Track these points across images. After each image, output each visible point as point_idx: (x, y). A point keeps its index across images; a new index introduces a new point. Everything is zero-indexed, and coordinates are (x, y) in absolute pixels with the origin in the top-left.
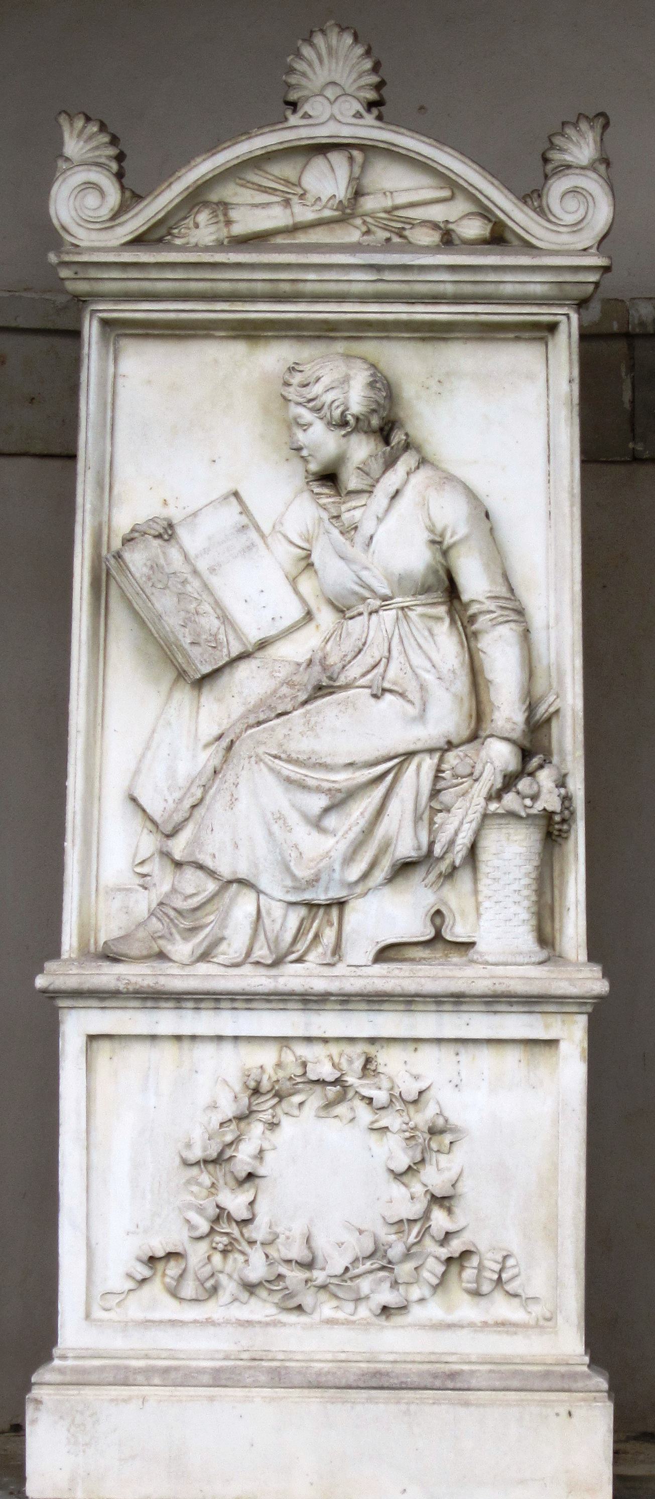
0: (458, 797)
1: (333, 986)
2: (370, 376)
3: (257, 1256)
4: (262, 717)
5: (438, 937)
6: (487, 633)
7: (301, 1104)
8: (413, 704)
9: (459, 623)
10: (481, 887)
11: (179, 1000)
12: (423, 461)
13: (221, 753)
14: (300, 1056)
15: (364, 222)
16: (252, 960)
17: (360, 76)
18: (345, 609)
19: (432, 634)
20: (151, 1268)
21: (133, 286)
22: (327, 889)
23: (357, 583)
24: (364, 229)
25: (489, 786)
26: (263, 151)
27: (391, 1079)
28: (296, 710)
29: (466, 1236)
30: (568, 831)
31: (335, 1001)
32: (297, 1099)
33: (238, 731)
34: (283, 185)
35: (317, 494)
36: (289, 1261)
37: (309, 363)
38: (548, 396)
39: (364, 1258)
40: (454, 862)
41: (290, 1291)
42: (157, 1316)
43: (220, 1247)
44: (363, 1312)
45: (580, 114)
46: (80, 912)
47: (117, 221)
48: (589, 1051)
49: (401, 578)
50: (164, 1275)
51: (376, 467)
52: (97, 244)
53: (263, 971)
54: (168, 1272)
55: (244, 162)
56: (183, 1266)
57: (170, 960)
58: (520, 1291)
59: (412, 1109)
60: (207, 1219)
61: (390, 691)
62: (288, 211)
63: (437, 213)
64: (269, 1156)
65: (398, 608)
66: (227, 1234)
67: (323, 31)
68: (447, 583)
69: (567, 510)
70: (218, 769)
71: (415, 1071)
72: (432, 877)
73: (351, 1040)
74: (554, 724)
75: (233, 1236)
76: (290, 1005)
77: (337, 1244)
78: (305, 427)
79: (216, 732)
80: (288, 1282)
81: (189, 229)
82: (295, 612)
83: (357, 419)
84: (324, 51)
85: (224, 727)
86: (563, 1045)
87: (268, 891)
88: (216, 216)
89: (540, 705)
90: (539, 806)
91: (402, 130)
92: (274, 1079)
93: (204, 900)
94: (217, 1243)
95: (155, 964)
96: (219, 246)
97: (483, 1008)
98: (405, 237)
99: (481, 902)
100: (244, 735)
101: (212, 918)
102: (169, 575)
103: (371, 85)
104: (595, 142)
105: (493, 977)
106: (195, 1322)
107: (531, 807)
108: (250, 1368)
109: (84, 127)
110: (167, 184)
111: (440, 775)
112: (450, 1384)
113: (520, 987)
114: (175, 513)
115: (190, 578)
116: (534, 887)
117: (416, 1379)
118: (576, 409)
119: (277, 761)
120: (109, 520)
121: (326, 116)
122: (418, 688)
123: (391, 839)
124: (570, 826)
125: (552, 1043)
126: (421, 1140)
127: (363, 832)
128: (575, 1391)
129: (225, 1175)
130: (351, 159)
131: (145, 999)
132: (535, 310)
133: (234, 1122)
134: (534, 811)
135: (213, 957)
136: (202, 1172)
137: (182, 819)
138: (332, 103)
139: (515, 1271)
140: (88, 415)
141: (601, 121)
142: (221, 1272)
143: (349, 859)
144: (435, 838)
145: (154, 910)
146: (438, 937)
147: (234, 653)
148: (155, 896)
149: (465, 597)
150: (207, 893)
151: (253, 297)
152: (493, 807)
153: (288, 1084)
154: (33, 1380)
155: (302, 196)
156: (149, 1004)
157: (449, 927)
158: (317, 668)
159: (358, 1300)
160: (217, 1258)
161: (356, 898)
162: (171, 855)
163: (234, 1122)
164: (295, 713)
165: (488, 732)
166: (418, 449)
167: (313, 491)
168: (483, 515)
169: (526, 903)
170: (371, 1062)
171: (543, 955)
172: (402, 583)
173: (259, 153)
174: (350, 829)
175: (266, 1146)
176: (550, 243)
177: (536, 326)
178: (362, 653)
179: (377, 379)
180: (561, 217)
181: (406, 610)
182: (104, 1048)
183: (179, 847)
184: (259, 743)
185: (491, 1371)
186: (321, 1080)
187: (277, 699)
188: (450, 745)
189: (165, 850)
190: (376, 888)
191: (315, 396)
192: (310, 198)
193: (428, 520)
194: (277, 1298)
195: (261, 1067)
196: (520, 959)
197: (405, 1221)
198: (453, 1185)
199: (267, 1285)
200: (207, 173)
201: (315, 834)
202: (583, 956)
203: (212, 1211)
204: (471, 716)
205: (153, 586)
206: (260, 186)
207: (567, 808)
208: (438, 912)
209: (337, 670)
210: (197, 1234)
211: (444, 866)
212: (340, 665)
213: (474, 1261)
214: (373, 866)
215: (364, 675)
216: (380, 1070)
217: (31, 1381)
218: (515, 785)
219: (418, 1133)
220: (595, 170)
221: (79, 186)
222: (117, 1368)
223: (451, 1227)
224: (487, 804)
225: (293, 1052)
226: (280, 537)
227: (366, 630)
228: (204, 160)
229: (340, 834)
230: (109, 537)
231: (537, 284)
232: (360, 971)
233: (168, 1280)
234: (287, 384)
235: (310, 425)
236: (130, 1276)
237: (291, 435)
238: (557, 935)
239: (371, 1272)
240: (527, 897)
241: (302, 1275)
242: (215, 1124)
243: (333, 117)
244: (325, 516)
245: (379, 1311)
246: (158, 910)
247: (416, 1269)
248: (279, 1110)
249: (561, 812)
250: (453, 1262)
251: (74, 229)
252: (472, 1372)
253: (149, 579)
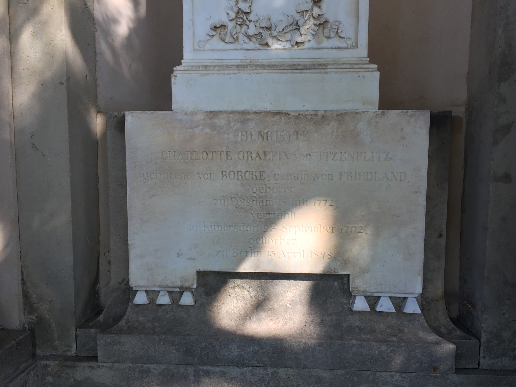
39: (289, 25)
66: (241, 18)
142: (240, 33)
160: (238, 27)
187: (268, 257)
203: (236, 10)
210: (231, 18)
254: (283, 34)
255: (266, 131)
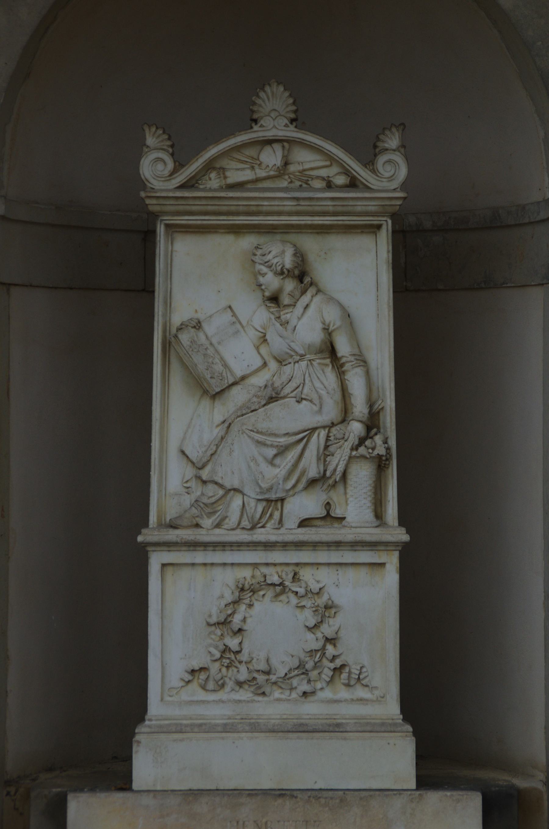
0: (337, 449)
1: (280, 539)
2: (294, 250)
3: (243, 669)
4: (244, 412)
5: (328, 515)
6: (350, 371)
7: (264, 595)
8: (316, 405)
9: (336, 367)
10: (348, 491)
11: (205, 546)
12: (319, 291)
13: (225, 429)
14: (263, 573)
15: (289, 177)
16: (241, 526)
17: (287, 106)
18: (282, 361)
19: (324, 372)
20: (192, 675)
21: (181, 208)
22: (276, 493)
23: (288, 349)
24: (289, 180)
25: (352, 443)
26: (241, 143)
27: (306, 583)
28: (260, 408)
29: (343, 657)
30: (389, 464)
31: (280, 546)
32: (262, 593)
33: (233, 419)
34: (250, 159)
35: (269, 307)
36: (258, 671)
37: (265, 244)
38: (377, 259)
40: (336, 479)
41: (259, 685)
42: (195, 698)
43: (226, 664)
44: (294, 695)
45: (392, 124)
46: (158, 506)
47: (172, 177)
48: (400, 568)
49: (309, 346)
50: (198, 678)
51: (297, 293)
52: (163, 188)
53: (246, 532)
54: (201, 677)
55: (232, 148)
56: (208, 674)
57: (201, 527)
58: (369, 684)
59: (316, 597)
60: (219, 651)
61: (305, 399)
62: (253, 172)
63: (323, 173)
64: (249, 620)
65: (308, 360)
66: (229, 658)
67: (269, 85)
68: (330, 348)
69: (386, 313)
70: (223, 437)
71: (317, 579)
72: (325, 487)
73: (287, 564)
74: (381, 414)
75: (232, 659)
76: (258, 548)
77: (281, 662)
78: (264, 275)
79: (222, 419)
80: (258, 680)
81: (206, 180)
82: (258, 363)
83: (288, 271)
84: (270, 95)
85: (226, 417)
86: (387, 566)
87: (248, 494)
88: (219, 174)
89: (374, 405)
90: (376, 452)
91: (307, 133)
92: (251, 583)
93: (218, 499)
94: (224, 663)
95: (194, 529)
96: (221, 189)
97: (350, 548)
98: (309, 184)
99: (348, 504)
100: (236, 421)
101: (221, 507)
102: (199, 346)
103: (292, 111)
104: (399, 137)
105: (355, 534)
106: (214, 701)
107: (372, 453)
108: (241, 723)
109: (156, 131)
110: (196, 159)
111: (329, 438)
112: (337, 730)
113: (368, 538)
114: (201, 316)
115: (209, 347)
116: (373, 491)
117: (320, 727)
118: (391, 265)
119: (252, 433)
120: (170, 319)
121: (271, 126)
122: (318, 397)
123: (306, 469)
124: (389, 462)
125: (382, 565)
126: (321, 612)
127: (293, 465)
128: (397, 732)
129: (227, 630)
130: (283, 147)
131: (190, 546)
132: (371, 218)
133: (231, 604)
134: (373, 455)
135: (222, 526)
136: (216, 628)
137: (206, 460)
138: (274, 120)
139: (366, 674)
140: (160, 269)
141: (402, 127)
142: (226, 677)
143: (287, 478)
144: (327, 468)
145: (193, 503)
146: (328, 515)
147: (230, 382)
148: (193, 497)
149: (339, 355)
150: (219, 495)
151: (238, 214)
152: (354, 453)
153: (258, 586)
154: (136, 731)
155: (260, 165)
156: (191, 548)
157: (333, 510)
158: (270, 389)
159: (292, 689)
160: (224, 670)
161: (290, 497)
162: (201, 478)
163: (231, 604)
164: (260, 410)
165: (351, 418)
166: (316, 286)
167: (267, 305)
168: (347, 316)
169: (370, 499)
170: (296, 574)
171: (378, 523)
172: (309, 348)
173: (239, 144)
174: (287, 464)
175: (247, 615)
176: (378, 186)
177: (371, 226)
178: (291, 382)
179: (297, 252)
180: (383, 174)
181: (312, 361)
182: (169, 571)
183: (205, 474)
184: (243, 424)
185: (356, 723)
186: (273, 583)
188: (333, 425)
189: (198, 475)
190: (299, 492)
191: (268, 260)
192: (264, 166)
193: (322, 318)
194: (252, 689)
195: (245, 578)
196: (367, 525)
197: (314, 651)
198: (336, 633)
199: (248, 682)
200: (215, 154)
201: (270, 467)
202: (396, 523)
203: (222, 647)
204: (342, 411)
205: (192, 350)
206: (240, 160)
207: (388, 454)
208: (328, 503)
209: (279, 390)
210: (214, 658)
211: (331, 482)
212: (281, 387)
213: (347, 670)
214: (298, 481)
215: (292, 392)
216: (301, 578)
217: (135, 732)
218: (364, 443)
219: (319, 608)
220: (399, 151)
221: (154, 159)
222: (176, 724)
223: (336, 653)
224: (351, 452)
225: (260, 571)
226: (251, 327)
227: (293, 371)
228: (213, 147)
229: (282, 467)
230: (170, 328)
231: (372, 206)
232: (291, 532)
233: (200, 681)
234: (255, 255)
235: (266, 274)
236: (182, 680)
237: (256, 279)
238: (384, 514)
239: (297, 675)
240: (370, 496)
241: (266, 677)
242: (223, 605)
243: (274, 127)
244: (273, 317)
245: (302, 694)
246: (195, 504)
247: (319, 674)
248: (253, 598)
249: (386, 456)
250: (338, 670)
251: (152, 180)
252: (347, 723)
253: (191, 347)
254: (286, 680)
255: (264, 820)
